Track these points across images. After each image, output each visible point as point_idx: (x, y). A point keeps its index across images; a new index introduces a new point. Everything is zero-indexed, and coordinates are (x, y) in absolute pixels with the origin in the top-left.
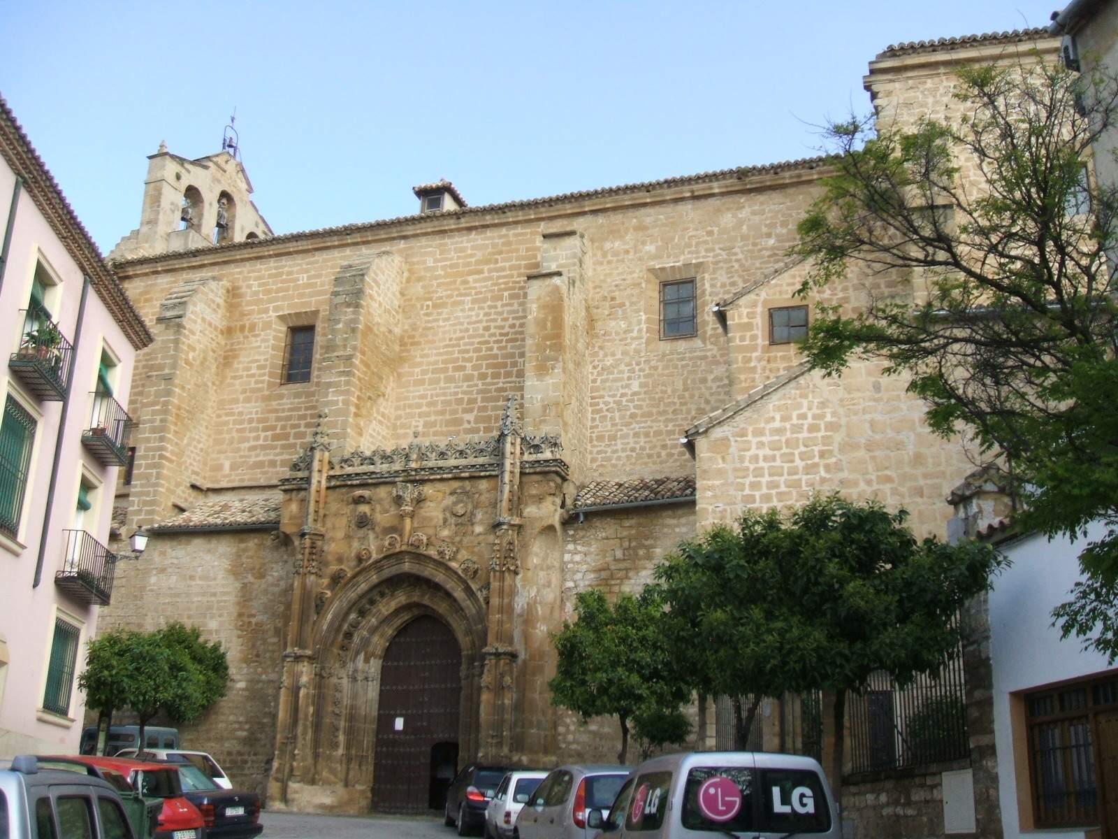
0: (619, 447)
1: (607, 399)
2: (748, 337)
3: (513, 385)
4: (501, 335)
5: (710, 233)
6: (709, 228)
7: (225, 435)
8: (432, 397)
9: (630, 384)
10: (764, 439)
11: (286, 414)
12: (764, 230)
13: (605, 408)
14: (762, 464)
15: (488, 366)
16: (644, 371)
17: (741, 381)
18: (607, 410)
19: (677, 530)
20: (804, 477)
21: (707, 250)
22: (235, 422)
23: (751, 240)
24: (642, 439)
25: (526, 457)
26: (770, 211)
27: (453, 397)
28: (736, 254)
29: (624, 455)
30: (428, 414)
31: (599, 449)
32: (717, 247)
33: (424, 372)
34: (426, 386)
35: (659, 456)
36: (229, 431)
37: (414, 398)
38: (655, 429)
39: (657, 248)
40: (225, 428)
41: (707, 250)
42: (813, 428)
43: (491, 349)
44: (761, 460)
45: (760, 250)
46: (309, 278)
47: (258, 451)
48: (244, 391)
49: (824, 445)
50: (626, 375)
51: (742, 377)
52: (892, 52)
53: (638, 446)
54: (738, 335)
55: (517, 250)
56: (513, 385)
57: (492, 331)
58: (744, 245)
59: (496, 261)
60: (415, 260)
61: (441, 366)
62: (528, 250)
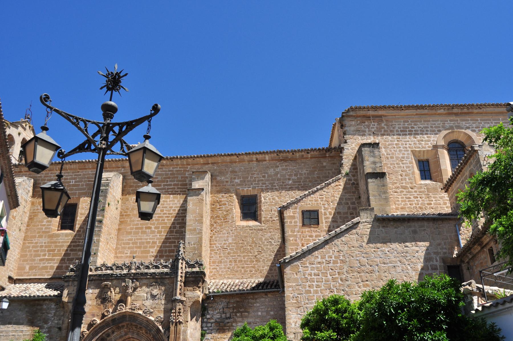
0: (223, 266)
1: (217, 245)
2: (293, 222)
3: (174, 237)
4: (169, 214)
5: (264, 177)
6: (263, 175)
7: (27, 253)
8: (135, 240)
9: (228, 239)
10: (314, 266)
11: (60, 244)
12: (287, 177)
13: (216, 249)
14: (313, 277)
15: (162, 227)
16: (234, 234)
17: (290, 241)
18: (218, 250)
19: (255, 305)
20: (332, 283)
21: (262, 184)
22: (33, 247)
23: (282, 181)
24: (233, 264)
25: (188, 270)
26: (290, 169)
27: (145, 241)
28: (275, 186)
29: (225, 270)
30: (133, 248)
31: (213, 267)
32: (267, 182)
33: (132, 229)
34: (132, 235)
35: (241, 271)
36: (30, 251)
37: (126, 240)
38: (239, 259)
39: (241, 181)
40: (28, 250)
41: (262, 184)
42: (335, 262)
43: (164, 220)
44: (313, 275)
45: (285, 185)
46: (75, 182)
47: (45, 261)
48: (39, 232)
49: (340, 269)
50: (226, 235)
51: (291, 239)
52: (352, 109)
53: (231, 267)
54: (289, 220)
55: (177, 177)
56: (174, 237)
57: (165, 212)
58: (279, 182)
59: (167, 182)
60: (129, 178)
61: (140, 226)
62: (182, 178)
